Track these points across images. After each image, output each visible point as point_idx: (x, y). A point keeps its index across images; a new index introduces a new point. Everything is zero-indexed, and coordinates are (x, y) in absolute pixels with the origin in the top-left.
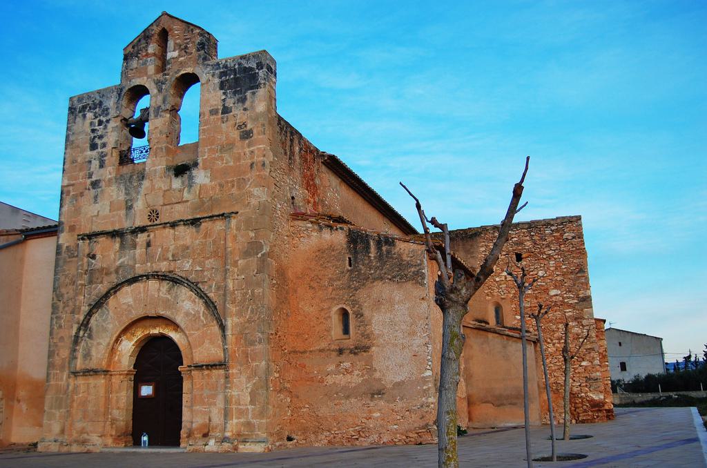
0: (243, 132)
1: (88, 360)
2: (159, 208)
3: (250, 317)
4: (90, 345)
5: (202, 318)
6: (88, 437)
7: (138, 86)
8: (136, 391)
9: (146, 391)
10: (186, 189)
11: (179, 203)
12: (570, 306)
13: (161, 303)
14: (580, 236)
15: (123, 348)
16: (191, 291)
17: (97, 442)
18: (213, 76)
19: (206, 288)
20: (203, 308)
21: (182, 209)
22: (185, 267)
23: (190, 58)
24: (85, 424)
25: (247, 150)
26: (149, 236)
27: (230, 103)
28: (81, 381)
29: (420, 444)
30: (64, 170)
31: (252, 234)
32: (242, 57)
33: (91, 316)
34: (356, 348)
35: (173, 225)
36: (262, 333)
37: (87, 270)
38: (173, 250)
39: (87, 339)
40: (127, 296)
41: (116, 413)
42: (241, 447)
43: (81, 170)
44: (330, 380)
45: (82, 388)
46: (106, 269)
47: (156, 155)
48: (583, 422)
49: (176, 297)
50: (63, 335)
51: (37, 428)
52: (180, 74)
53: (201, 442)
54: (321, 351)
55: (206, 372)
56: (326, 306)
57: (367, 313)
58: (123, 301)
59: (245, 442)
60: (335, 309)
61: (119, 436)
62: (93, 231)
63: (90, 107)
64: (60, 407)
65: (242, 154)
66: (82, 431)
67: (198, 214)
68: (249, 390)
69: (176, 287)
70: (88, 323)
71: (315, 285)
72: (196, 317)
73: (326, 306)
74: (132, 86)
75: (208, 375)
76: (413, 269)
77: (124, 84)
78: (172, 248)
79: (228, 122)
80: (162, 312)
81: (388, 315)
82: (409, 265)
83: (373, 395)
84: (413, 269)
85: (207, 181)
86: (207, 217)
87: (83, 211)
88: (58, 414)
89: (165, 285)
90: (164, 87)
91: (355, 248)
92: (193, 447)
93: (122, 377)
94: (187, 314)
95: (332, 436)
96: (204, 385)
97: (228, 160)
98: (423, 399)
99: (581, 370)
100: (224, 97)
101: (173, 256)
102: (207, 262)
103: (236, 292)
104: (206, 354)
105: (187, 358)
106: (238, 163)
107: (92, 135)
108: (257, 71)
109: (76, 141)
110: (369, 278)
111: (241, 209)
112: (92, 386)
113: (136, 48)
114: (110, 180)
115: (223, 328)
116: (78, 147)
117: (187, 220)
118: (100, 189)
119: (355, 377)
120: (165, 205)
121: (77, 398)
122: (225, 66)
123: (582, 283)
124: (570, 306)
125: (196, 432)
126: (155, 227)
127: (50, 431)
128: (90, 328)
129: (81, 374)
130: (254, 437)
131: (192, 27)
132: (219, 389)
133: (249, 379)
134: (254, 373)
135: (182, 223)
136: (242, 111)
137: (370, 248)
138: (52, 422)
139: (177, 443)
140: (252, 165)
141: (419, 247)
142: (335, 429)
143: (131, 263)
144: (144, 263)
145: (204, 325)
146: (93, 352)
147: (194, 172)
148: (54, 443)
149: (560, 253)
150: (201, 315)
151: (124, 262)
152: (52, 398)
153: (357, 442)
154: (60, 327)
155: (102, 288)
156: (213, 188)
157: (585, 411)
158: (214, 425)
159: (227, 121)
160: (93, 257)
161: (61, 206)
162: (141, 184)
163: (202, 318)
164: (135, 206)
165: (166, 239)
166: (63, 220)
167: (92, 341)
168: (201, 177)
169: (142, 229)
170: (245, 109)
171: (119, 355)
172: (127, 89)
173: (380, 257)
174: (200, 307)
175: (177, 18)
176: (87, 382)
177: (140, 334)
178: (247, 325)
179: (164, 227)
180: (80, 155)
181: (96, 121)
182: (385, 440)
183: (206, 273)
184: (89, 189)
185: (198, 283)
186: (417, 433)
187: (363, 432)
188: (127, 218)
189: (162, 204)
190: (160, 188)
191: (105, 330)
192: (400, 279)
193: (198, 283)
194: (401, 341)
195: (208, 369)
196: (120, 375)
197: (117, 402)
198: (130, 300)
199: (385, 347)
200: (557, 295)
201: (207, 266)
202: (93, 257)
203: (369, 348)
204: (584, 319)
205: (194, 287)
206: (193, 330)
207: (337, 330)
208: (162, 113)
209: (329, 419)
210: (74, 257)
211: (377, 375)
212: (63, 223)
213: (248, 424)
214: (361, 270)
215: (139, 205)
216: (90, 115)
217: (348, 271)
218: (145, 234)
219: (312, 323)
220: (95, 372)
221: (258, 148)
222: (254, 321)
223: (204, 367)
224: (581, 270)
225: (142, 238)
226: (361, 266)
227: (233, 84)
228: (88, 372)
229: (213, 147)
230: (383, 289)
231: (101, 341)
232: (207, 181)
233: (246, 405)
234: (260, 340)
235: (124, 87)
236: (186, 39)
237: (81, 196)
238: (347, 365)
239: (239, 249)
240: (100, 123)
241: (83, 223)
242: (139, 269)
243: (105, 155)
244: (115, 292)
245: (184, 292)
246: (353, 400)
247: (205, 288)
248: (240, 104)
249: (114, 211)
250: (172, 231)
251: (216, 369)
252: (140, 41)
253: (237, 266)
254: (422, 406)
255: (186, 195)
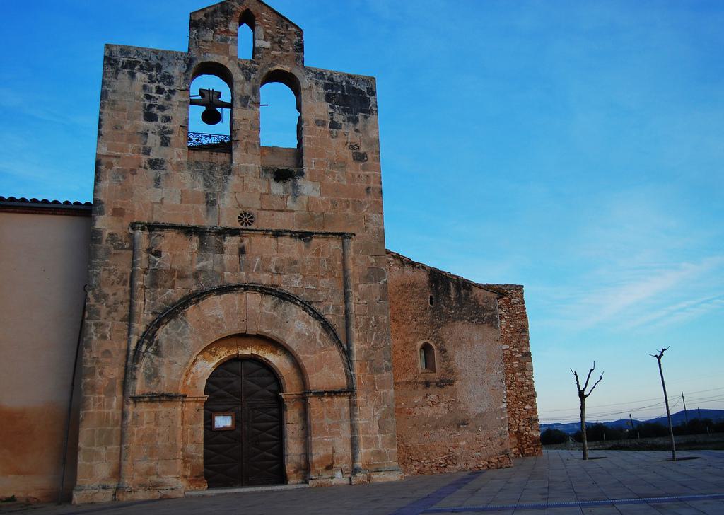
0: (356, 153)
1: (155, 383)
2: (255, 212)
3: (375, 344)
4: (156, 363)
5: (318, 340)
6: (160, 480)
7: (210, 62)
8: (209, 422)
9: (223, 422)
10: (290, 197)
11: (282, 211)
12: (517, 359)
13: (264, 319)
14: (523, 302)
15: (199, 370)
16: (304, 310)
17: (177, 483)
18: (317, 83)
19: (322, 309)
20: (319, 331)
21: (286, 219)
22: (293, 283)
23: (287, 55)
24: (153, 464)
25: (362, 173)
26: (241, 241)
27: (339, 118)
28: (144, 409)
29: (501, 468)
30: (99, 135)
31: (372, 260)
32: (349, 76)
33: (158, 328)
34: (442, 381)
35: (277, 234)
36: (389, 361)
37: (147, 269)
38: (277, 262)
39: (152, 356)
40: (215, 307)
41: (191, 448)
42: (375, 476)
43: (130, 140)
44: (417, 412)
45: (146, 418)
46: (179, 271)
47: (246, 150)
48: (527, 455)
49: (284, 315)
50: (110, 349)
51: (13, 476)
52: (277, 68)
53: (326, 475)
54: (408, 383)
55: (326, 400)
56: (411, 339)
57: (450, 349)
58: (207, 312)
59: (377, 471)
60: (420, 344)
61: (196, 477)
62: (154, 221)
63: (141, 66)
64: (108, 442)
65: (356, 176)
66: (149, 472)
67: (307, 227)
68: (377, 418)
69: (283, 305)
70: (154, 335)
71: (399, 318)
72: (311, 340)
73: (411, 339)
74: (208, 60)
75: (328, 402)
76: (488, 314)
77: (194, 53)
78: (274, 259)
79: (337, 139)
80: (265, 330)
81: (469, 352)
82: (484, 309)
83: (459, 425)
84: (488, 314)
85: (316, 194)
86: (321, 233)
87: (136, 192)
88: (103, 452)
89: (269, 302)
90: (252, 76)
91: (436, 288)
92: (318, 481)
93: (198, 404)
94: (300, 335)
95: (422, 465)
96: (325, 413)
97: (339, 178)
98: (502, 428)
99: (525, 412)
100: (331, 111)
101: (277, 268)
102: (321, 281)
103: (358, 317)
104: (325, 381)
105: (291, 383)
106: (352, 184)
107: (148, 103)
108: (368, 96)
109: (119, 103)
110: (450, 317)
111: (358, 232)
112: (163, 414)
113: (210, 19)
114: (179, 164)
115: (347, 353)
116: (124, 110)
117: (296, 232)
118: (164, 172)
119: (441, 408)
120: (262, 209)
121: (138, 431)
122: (330, 79)
123: (525, 341)
124: (517, 359)
125: (316, 465)
126: (253, 232)
127: (91, 475)
128: (157, 342)
129: (147, 399)
130: (386, 466)
131: (286, 23)
132: (343, 417)
133: (377, 407)
134: (382, 401)
135: (289, 234)
136: (354, 132)
137: (450, 290)
138: (94, 463)
139: (287, 484)
140: (368, 189)
141: (492, 294)
142: (425, 458)
143: (216, 268)
144: (236, 271)
145: (322, 349)
146: (164, 372)
147: (300, 181)
148: (102, 491)
149: (509, 314)
150: (318, 337)
151: (206, 266)
152: (94, 431)
153: (446, 470)
154: (104, 337)
155: (175, 293)
156: (324, 204)
157: (528, 446)
158: (339, 456)
159: (337, 136)
160: (158, 254)
161: (97, 180)
162: (226, 179)
163: (318, 340)
164: (220, 202)
165: (263, 247)
166: (101, 197)
167: (160, 359)
168: (307, 188)
169: (234, 232)
170: (357, 131)
171: (193, 378)
172: (200, 61)
173: (459, 299)
174: (316, 328)
175: (266, 5)
176: (156, 410)
177: (223, 354)
178: (371, 352)
179: (264, 235)
180: (128, 121)
181: (153, 86)
182: (471, 466)
183: (320, 293)
184: (145, 168)
185: (312, 302)
186: (498, 458)
187: (450, 460)
188: (208, 215)
189: (260, 208)
190: (255, 189)
191: (181, 346)
192: (478, 321)
193: (311, 303)
194: (481, 377)
195: (329, 396)
196: (196, 402)
197: (192, 435)
198: (221, 313)
199: (467, 381)
200: (507, 349)
201: (321, 285)
202: (158, 254)
203: (453, 381)
204: (527, 370)
205: (306, 306)
206: (308, 353)
207: (420, 365)
208: (252, 105)
209: (419, 449)
210: (123, 249)
211: (462, 407)
212: (101, 203)
213: (379, 453)
214: (442, 308)
215: (226, 202)
216: (141, 77)
217: (431, 308)
218: (237, 238)
219: (397, 356)
220: (170, 398)
221: (374, 174)
222: (380, 348)
223: (326, 394)
224: (524, 330)
225: (231, 242)
226: (442, 305)
227: (341, 101)
228: (155, 398)
229: (322, 159)
230: (461, 329)
231: (175, 359)
232: (316, 194)
233: (375, 434)
234: (387, 368)
235: (195, 59)
236: (279, 33)
237: (133, 174)
238: (433, 397)
239: (359, 272)
240: (160, 91)
241: (137, 209)
242: (230, 278)
243: (171, 132)
244: (197, 302)
245: (295, 311)
246: (441, 430)
247: (320, 309)
248: (351, 124)
249: (188, 202)
250: (274, 241)
251: (340, 396)
252: (215, 11)
253: (358, 290)
254: (501, 435)
255: (290, 204)
